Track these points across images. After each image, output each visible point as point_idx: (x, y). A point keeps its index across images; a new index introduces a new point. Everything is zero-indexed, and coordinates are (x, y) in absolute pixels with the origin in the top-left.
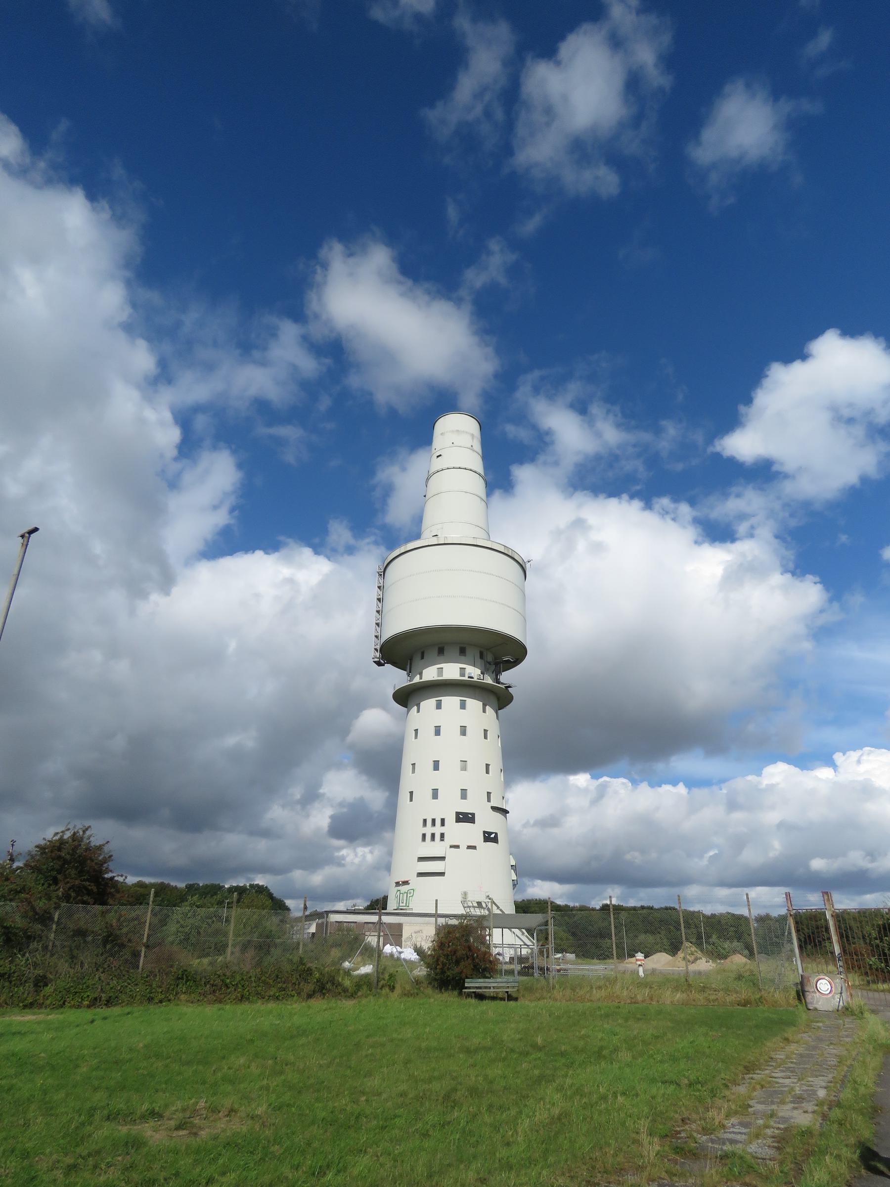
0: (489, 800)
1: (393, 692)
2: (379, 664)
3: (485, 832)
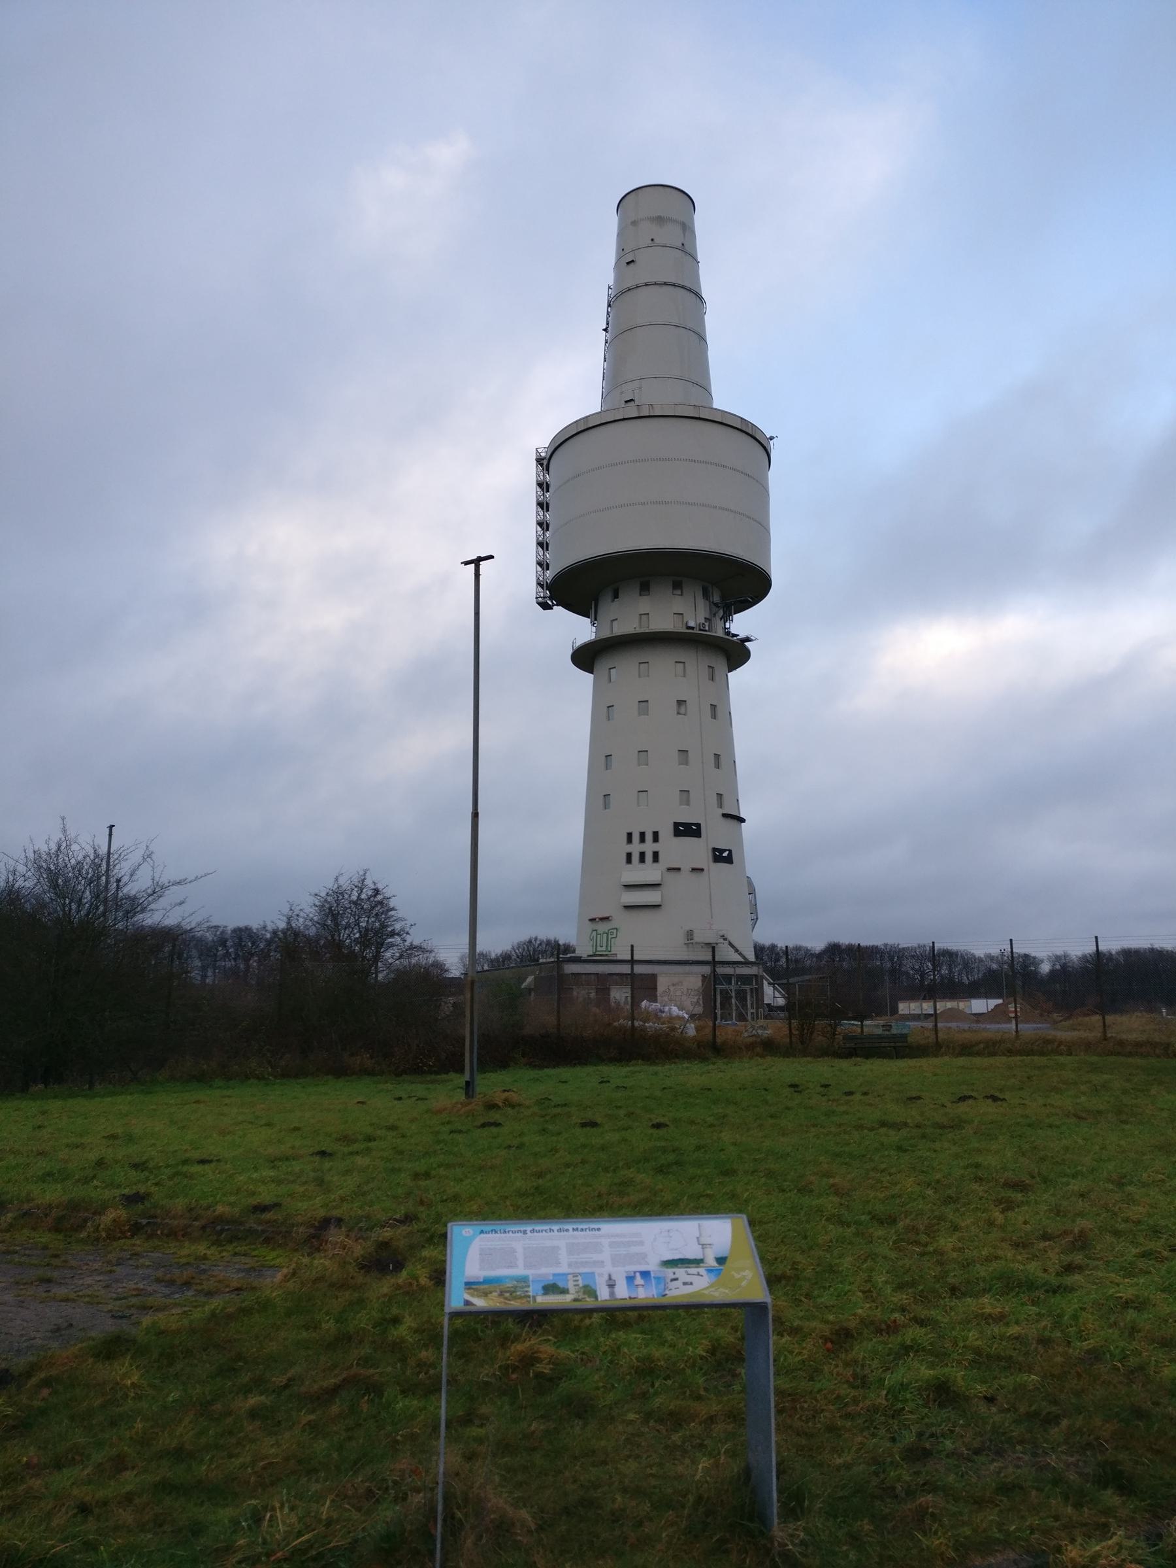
0: (721, 806)
1: (571, 651)
2: (545, 606)
3: (714, 850)
